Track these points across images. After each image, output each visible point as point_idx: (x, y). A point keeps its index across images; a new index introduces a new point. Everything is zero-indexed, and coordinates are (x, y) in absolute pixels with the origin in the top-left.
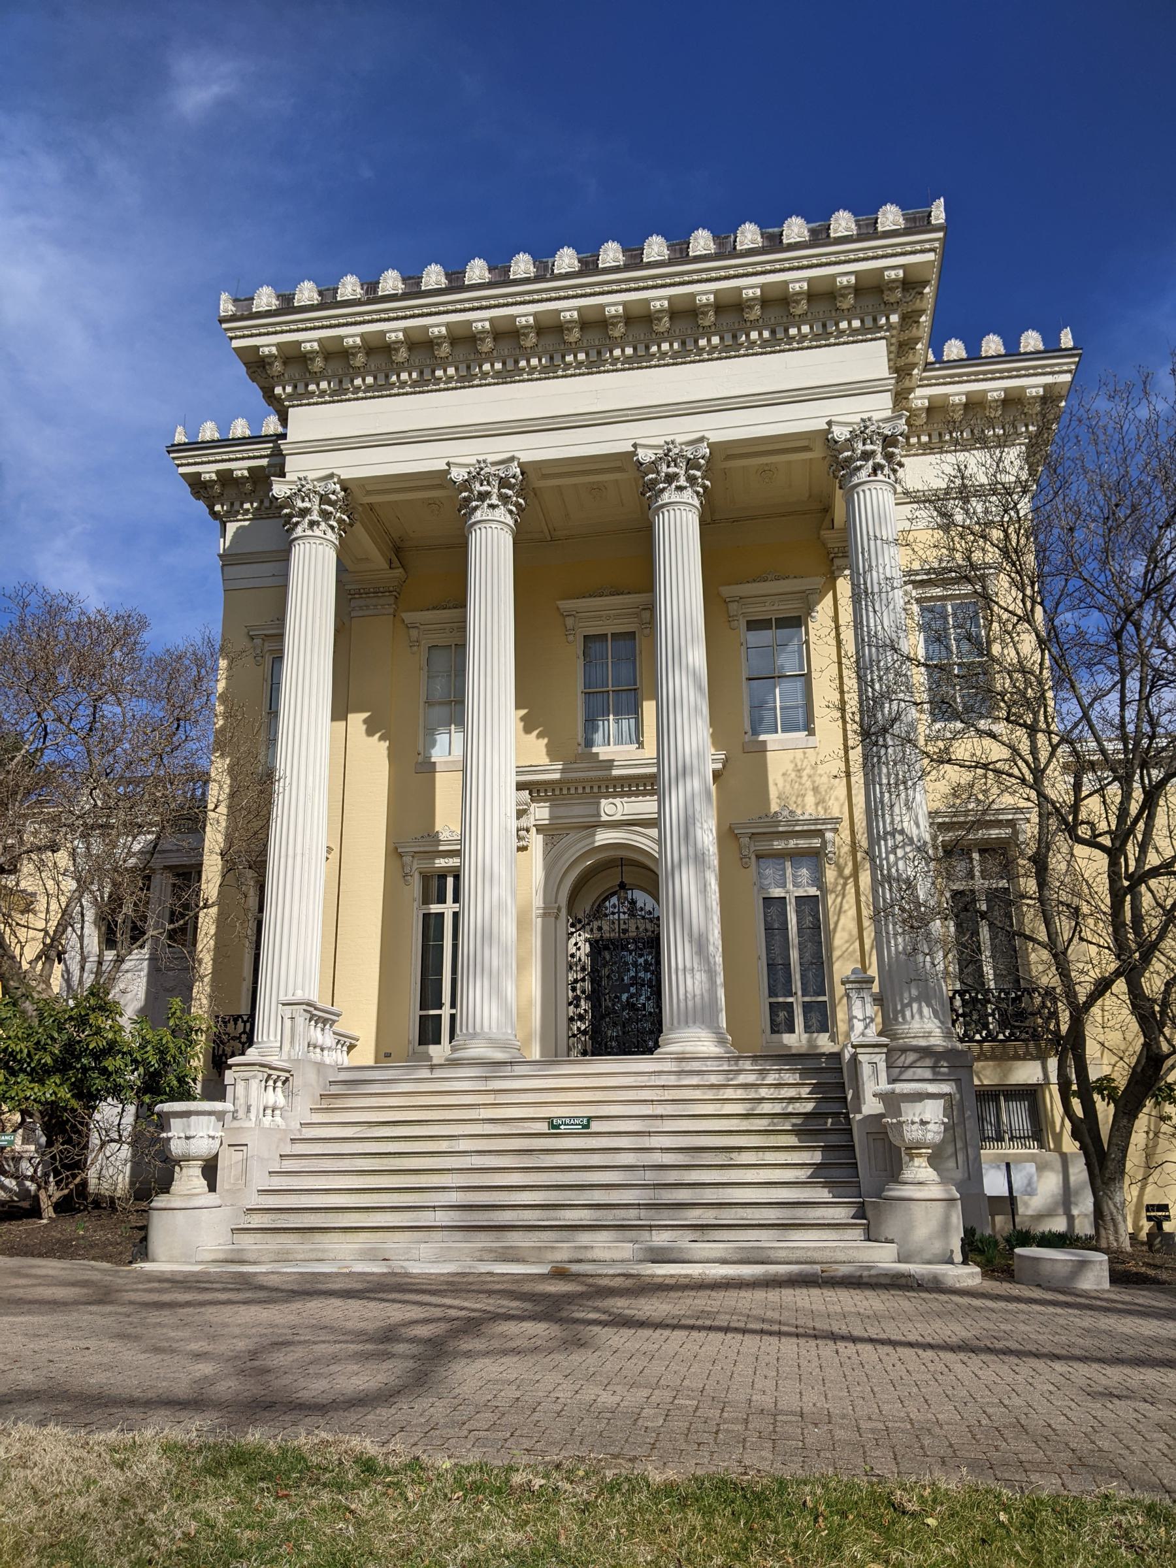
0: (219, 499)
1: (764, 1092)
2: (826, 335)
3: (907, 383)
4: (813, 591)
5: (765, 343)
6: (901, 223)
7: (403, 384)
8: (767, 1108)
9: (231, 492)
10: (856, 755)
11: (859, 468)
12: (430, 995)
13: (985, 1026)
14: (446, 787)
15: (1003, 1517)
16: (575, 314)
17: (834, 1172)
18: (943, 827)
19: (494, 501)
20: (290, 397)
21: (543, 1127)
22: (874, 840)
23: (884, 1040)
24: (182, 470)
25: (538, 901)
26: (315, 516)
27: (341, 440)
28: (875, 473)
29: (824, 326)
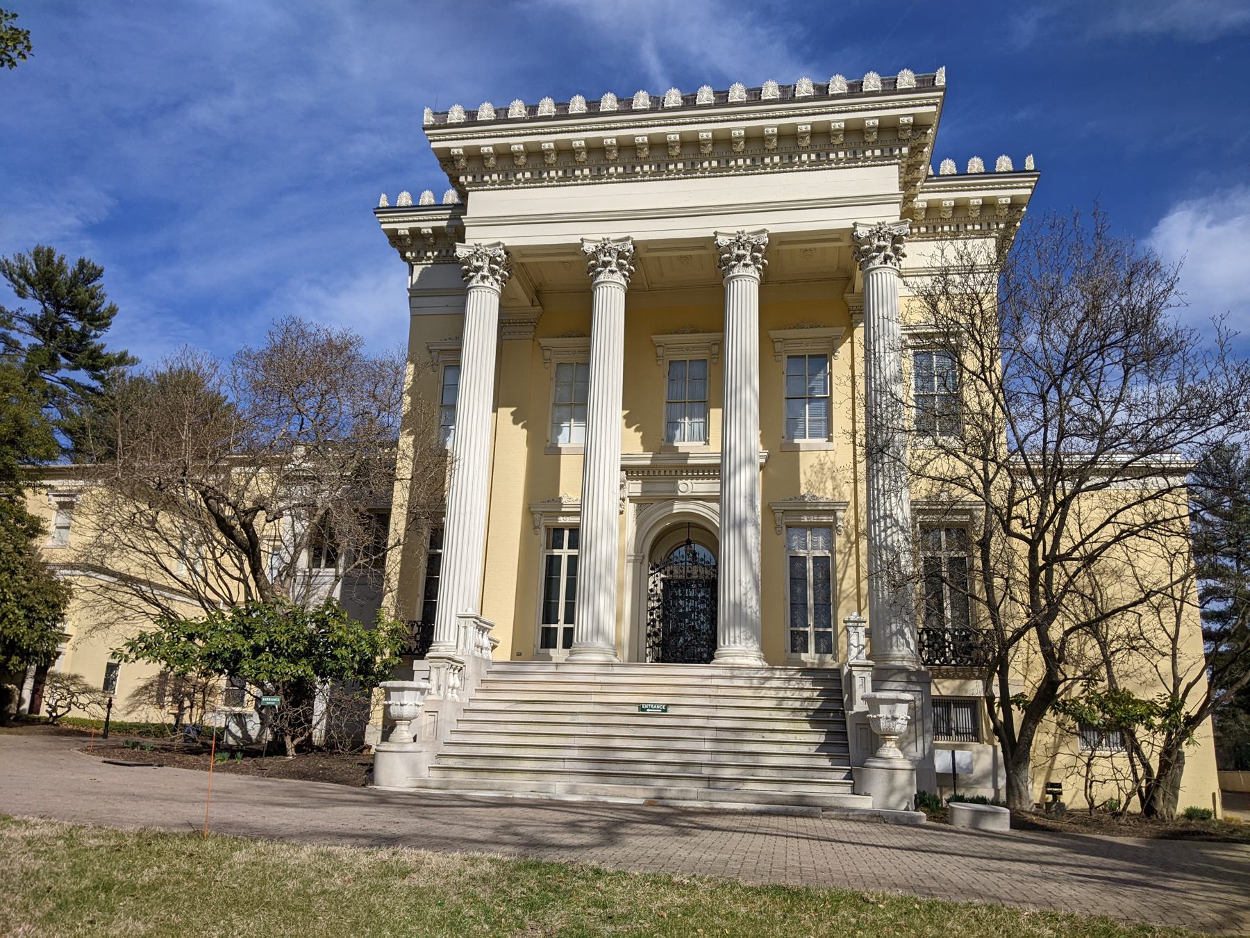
0: (410, 248)
1: (789, 694)
2: (856, 159)
3: (912, 191)
4: (837, 337)
5: (812, 163)
6: (914, 84)
7: (552, 179)
8: (789, 704)
9: (419, 243)
10: (862, 467)
11: (874, 258)
12: (549, 614)
13: (944, 654)
14: (569, 469)
15: (917, 906)
16: (678, 137)
17: (832, 749)
18: (920, 511)
19: (614, 268)
20: (470, 184)
21: (635, 710)
22: (871, 522)
23: (871, 662)
24: (384, 226)
25: (631, 550)
26: (486, 272)
27: (506, 217)
28: (885, 261)
29: (855, 153)
